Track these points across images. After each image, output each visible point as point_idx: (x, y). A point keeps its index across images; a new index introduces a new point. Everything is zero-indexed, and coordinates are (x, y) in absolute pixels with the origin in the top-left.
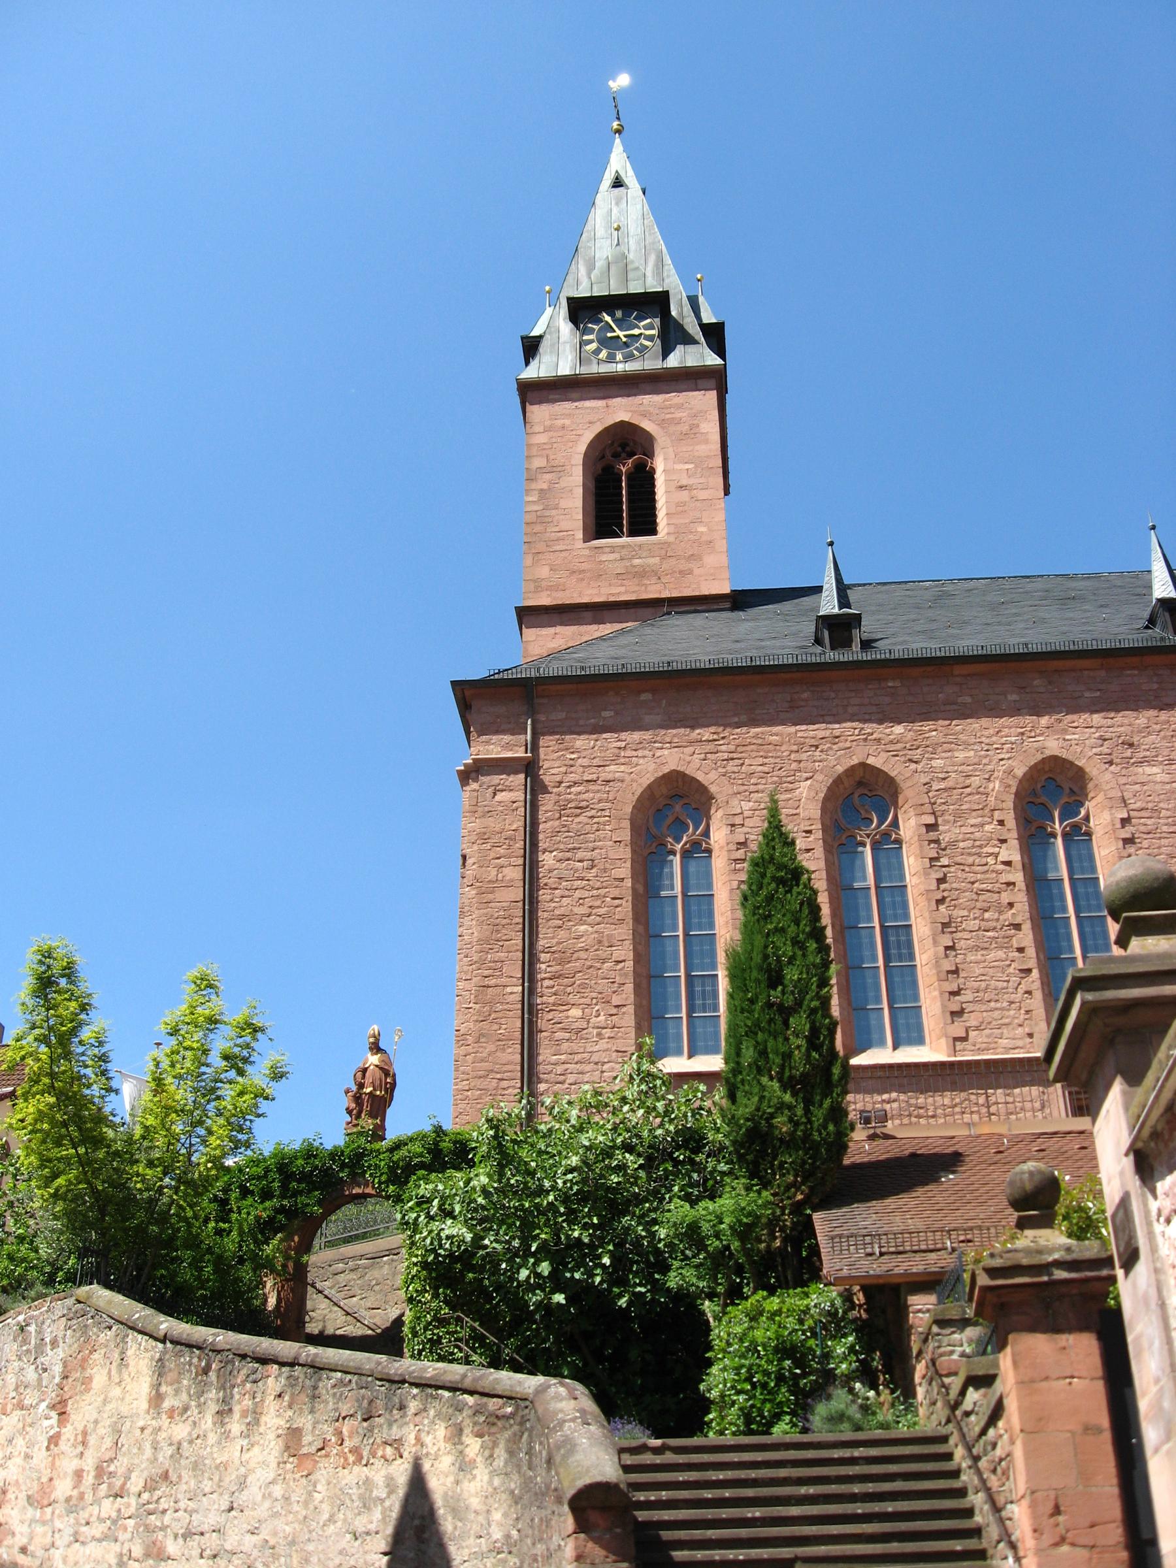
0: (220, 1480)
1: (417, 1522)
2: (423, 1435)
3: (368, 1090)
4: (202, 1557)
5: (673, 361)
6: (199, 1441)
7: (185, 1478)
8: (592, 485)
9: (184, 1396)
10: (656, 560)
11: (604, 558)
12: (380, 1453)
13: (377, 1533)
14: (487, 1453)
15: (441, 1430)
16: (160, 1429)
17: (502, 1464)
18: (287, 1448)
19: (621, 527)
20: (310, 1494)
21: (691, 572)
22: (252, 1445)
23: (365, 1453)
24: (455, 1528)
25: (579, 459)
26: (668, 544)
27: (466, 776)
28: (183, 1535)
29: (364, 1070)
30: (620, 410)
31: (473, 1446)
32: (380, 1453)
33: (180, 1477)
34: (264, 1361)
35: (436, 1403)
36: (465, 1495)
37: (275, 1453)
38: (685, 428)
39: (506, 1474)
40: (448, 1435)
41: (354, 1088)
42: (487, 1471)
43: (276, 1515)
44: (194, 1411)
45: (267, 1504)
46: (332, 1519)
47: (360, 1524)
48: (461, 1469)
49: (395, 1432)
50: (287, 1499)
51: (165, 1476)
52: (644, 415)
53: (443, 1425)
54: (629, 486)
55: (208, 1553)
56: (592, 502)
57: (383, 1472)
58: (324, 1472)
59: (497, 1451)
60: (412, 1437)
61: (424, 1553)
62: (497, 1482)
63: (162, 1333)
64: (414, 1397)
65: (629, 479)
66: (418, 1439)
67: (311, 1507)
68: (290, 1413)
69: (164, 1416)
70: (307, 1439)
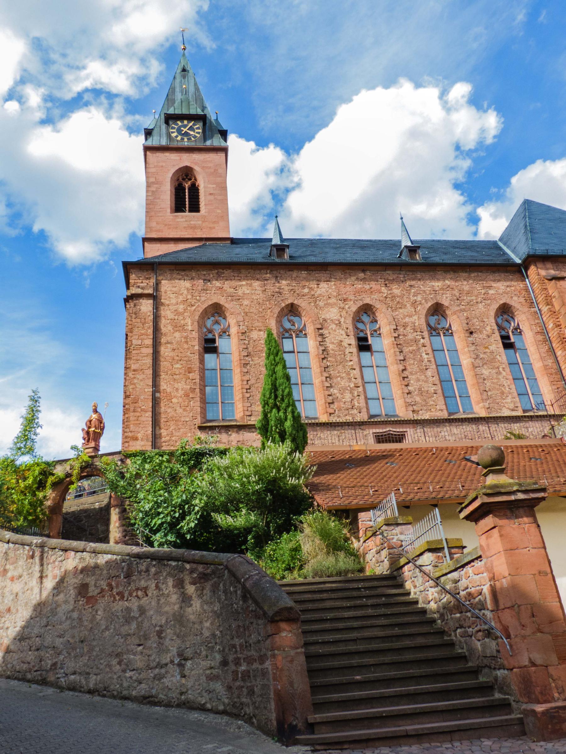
0: (41, 611)
1: (157, 628)
2: (160, 585)
3: (93, 429)
4: (30, 650)
5: (208, 143)
6: (29, 592)
7: (20, 610)
8: (174, 191)
9: (20, 570)
10: (200, 222)
11: (179, 220)
12: (135, 594)
13: (134, 635)
14: (199, 592)
15: (170, 582)
16: (6, 587)
17: (208, 598)
18: (80, 593)
19: (185, 208)
20: (94, 616)
21: (214, 228)
22: (60, 593)
23: (126, 595)
24: (181, 631)
25: (169, 180)
26: (205, 216)
27: (127, 300)
28: (19, 639)
29: (90, 421)
30: (186, 160)
31: (191, 589)
32: (135, 594)
33: (17, 610)
34: (65, 550)
35: (168, 569)
36: (186, 614)
37: (73, 596)
38: (212, 170)
39: (211, 603)
40: (175, 583)
41: (86, 429)
42: (199, 602)
43: (73, 627)
44: (25, 577)
45: (68, 622)
46: (107, 628)
47: (125, 630)
48: (183, 601)
49: (143, 583)
50: (80, 619)
51: (9, 610)
52: (196, 164)
53: (172, 579)
54: (189, 192)
55: (34, 648)
56: (174, 197)
57: (136, 604)
58: (102, 605)
59: (205, 592)
60: (154, 585)
61: (162, 644)
62: (205, 607)
63: (7, 540)
64: (154, 566)
65: (189, 189)
66: (157, 587)
67: (95, 623)
68: (81, 576)
69: (8, 581)
70: (91, 588)
